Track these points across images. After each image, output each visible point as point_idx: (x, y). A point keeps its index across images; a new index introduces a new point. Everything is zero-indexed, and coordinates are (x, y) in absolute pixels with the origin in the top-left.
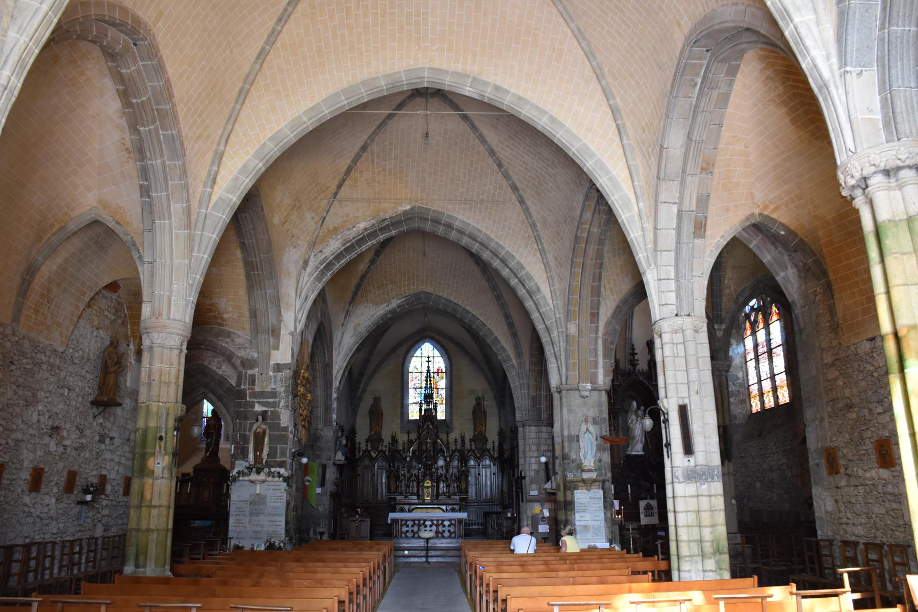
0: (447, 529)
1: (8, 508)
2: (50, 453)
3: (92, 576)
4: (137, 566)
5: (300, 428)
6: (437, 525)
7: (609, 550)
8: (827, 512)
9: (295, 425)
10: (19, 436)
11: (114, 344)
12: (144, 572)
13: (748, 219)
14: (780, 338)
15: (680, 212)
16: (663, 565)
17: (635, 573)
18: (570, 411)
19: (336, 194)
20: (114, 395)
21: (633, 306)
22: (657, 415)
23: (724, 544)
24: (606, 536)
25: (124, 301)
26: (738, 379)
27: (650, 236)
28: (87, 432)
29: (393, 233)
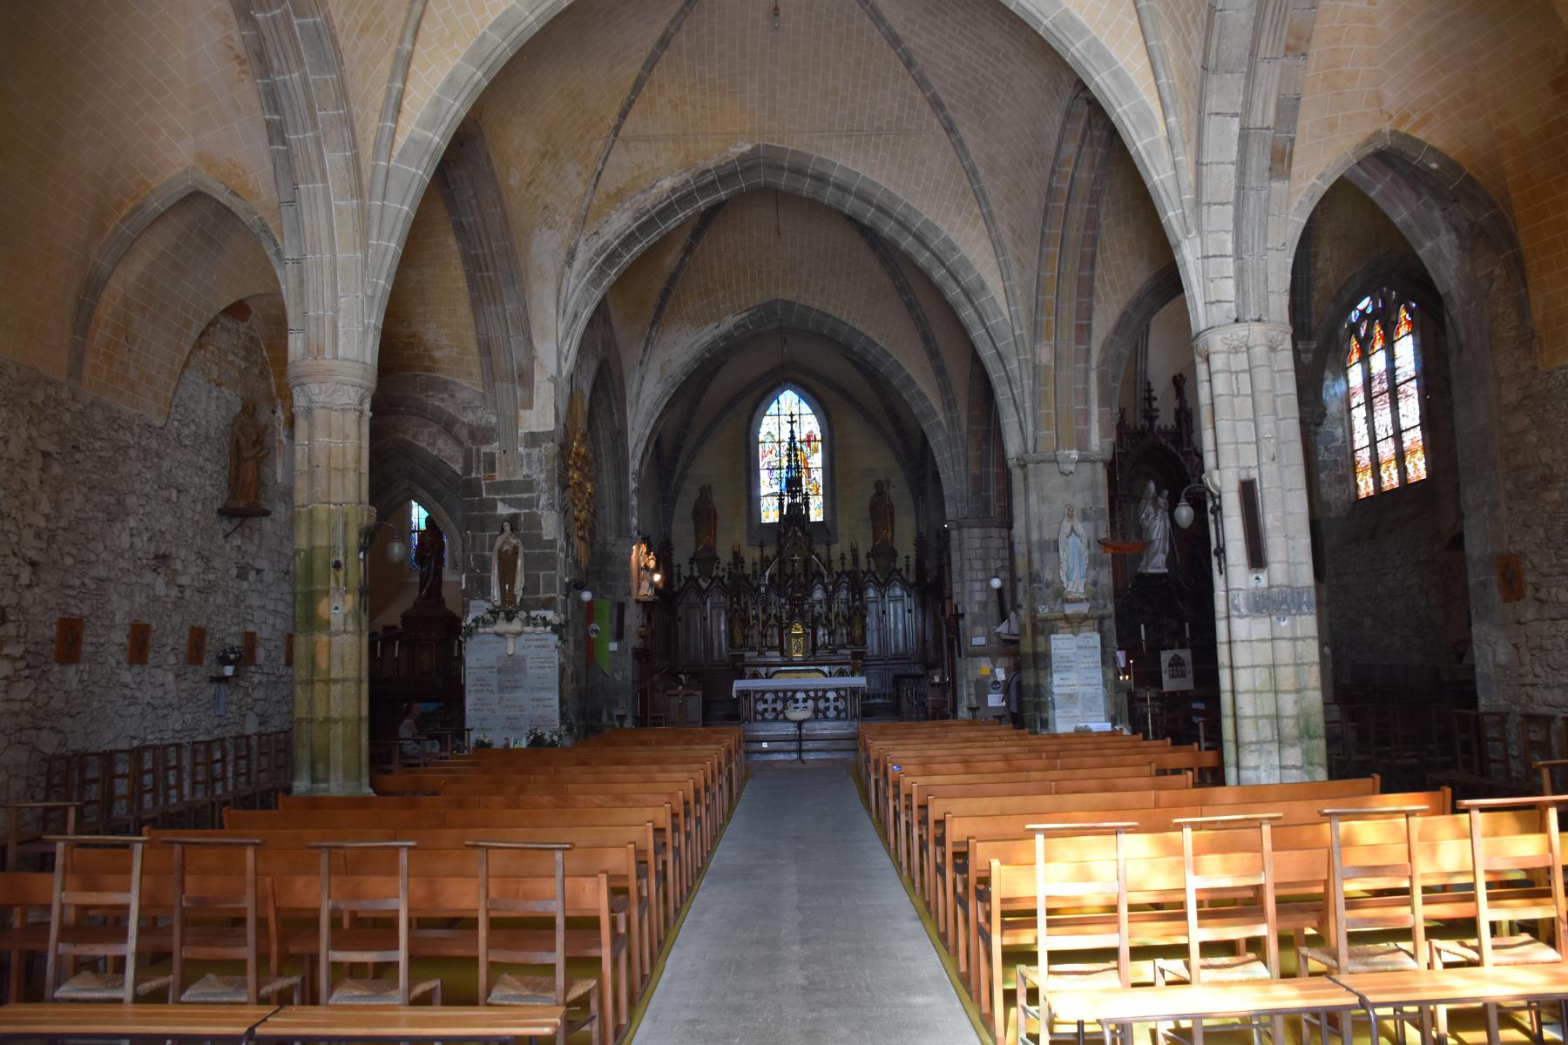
0: (832, 704)
1: (97, 691)
2: (156, 599)
3: (246, 797)
4: (314, 780)
5: (577, 542)
6: (816, 699)
7: (1113, 733)
8: (1497, 666)
9: (568, 537)
10: (102, 571)
11: (249, 409)
12: (327, 790)
13: (1369, 141)
14: (1413, 365)
15: (1244, 136)
16: (1209, 759)
17: (1162, 772)
18: (1043, 499)
19: (617, 128)
20: (257, 497)
21: (1152, 312)
22: (1204, 503)
23: (1318, 721)
24: (1107, 712)
25: (255, 331)
26: (1334, 439)
27: (1188, 177)
28: (217, 562)
29: (723, 194)
